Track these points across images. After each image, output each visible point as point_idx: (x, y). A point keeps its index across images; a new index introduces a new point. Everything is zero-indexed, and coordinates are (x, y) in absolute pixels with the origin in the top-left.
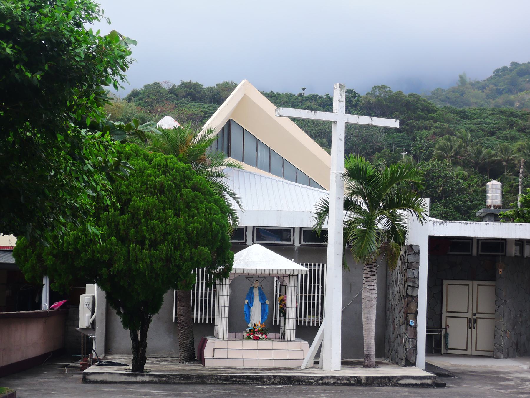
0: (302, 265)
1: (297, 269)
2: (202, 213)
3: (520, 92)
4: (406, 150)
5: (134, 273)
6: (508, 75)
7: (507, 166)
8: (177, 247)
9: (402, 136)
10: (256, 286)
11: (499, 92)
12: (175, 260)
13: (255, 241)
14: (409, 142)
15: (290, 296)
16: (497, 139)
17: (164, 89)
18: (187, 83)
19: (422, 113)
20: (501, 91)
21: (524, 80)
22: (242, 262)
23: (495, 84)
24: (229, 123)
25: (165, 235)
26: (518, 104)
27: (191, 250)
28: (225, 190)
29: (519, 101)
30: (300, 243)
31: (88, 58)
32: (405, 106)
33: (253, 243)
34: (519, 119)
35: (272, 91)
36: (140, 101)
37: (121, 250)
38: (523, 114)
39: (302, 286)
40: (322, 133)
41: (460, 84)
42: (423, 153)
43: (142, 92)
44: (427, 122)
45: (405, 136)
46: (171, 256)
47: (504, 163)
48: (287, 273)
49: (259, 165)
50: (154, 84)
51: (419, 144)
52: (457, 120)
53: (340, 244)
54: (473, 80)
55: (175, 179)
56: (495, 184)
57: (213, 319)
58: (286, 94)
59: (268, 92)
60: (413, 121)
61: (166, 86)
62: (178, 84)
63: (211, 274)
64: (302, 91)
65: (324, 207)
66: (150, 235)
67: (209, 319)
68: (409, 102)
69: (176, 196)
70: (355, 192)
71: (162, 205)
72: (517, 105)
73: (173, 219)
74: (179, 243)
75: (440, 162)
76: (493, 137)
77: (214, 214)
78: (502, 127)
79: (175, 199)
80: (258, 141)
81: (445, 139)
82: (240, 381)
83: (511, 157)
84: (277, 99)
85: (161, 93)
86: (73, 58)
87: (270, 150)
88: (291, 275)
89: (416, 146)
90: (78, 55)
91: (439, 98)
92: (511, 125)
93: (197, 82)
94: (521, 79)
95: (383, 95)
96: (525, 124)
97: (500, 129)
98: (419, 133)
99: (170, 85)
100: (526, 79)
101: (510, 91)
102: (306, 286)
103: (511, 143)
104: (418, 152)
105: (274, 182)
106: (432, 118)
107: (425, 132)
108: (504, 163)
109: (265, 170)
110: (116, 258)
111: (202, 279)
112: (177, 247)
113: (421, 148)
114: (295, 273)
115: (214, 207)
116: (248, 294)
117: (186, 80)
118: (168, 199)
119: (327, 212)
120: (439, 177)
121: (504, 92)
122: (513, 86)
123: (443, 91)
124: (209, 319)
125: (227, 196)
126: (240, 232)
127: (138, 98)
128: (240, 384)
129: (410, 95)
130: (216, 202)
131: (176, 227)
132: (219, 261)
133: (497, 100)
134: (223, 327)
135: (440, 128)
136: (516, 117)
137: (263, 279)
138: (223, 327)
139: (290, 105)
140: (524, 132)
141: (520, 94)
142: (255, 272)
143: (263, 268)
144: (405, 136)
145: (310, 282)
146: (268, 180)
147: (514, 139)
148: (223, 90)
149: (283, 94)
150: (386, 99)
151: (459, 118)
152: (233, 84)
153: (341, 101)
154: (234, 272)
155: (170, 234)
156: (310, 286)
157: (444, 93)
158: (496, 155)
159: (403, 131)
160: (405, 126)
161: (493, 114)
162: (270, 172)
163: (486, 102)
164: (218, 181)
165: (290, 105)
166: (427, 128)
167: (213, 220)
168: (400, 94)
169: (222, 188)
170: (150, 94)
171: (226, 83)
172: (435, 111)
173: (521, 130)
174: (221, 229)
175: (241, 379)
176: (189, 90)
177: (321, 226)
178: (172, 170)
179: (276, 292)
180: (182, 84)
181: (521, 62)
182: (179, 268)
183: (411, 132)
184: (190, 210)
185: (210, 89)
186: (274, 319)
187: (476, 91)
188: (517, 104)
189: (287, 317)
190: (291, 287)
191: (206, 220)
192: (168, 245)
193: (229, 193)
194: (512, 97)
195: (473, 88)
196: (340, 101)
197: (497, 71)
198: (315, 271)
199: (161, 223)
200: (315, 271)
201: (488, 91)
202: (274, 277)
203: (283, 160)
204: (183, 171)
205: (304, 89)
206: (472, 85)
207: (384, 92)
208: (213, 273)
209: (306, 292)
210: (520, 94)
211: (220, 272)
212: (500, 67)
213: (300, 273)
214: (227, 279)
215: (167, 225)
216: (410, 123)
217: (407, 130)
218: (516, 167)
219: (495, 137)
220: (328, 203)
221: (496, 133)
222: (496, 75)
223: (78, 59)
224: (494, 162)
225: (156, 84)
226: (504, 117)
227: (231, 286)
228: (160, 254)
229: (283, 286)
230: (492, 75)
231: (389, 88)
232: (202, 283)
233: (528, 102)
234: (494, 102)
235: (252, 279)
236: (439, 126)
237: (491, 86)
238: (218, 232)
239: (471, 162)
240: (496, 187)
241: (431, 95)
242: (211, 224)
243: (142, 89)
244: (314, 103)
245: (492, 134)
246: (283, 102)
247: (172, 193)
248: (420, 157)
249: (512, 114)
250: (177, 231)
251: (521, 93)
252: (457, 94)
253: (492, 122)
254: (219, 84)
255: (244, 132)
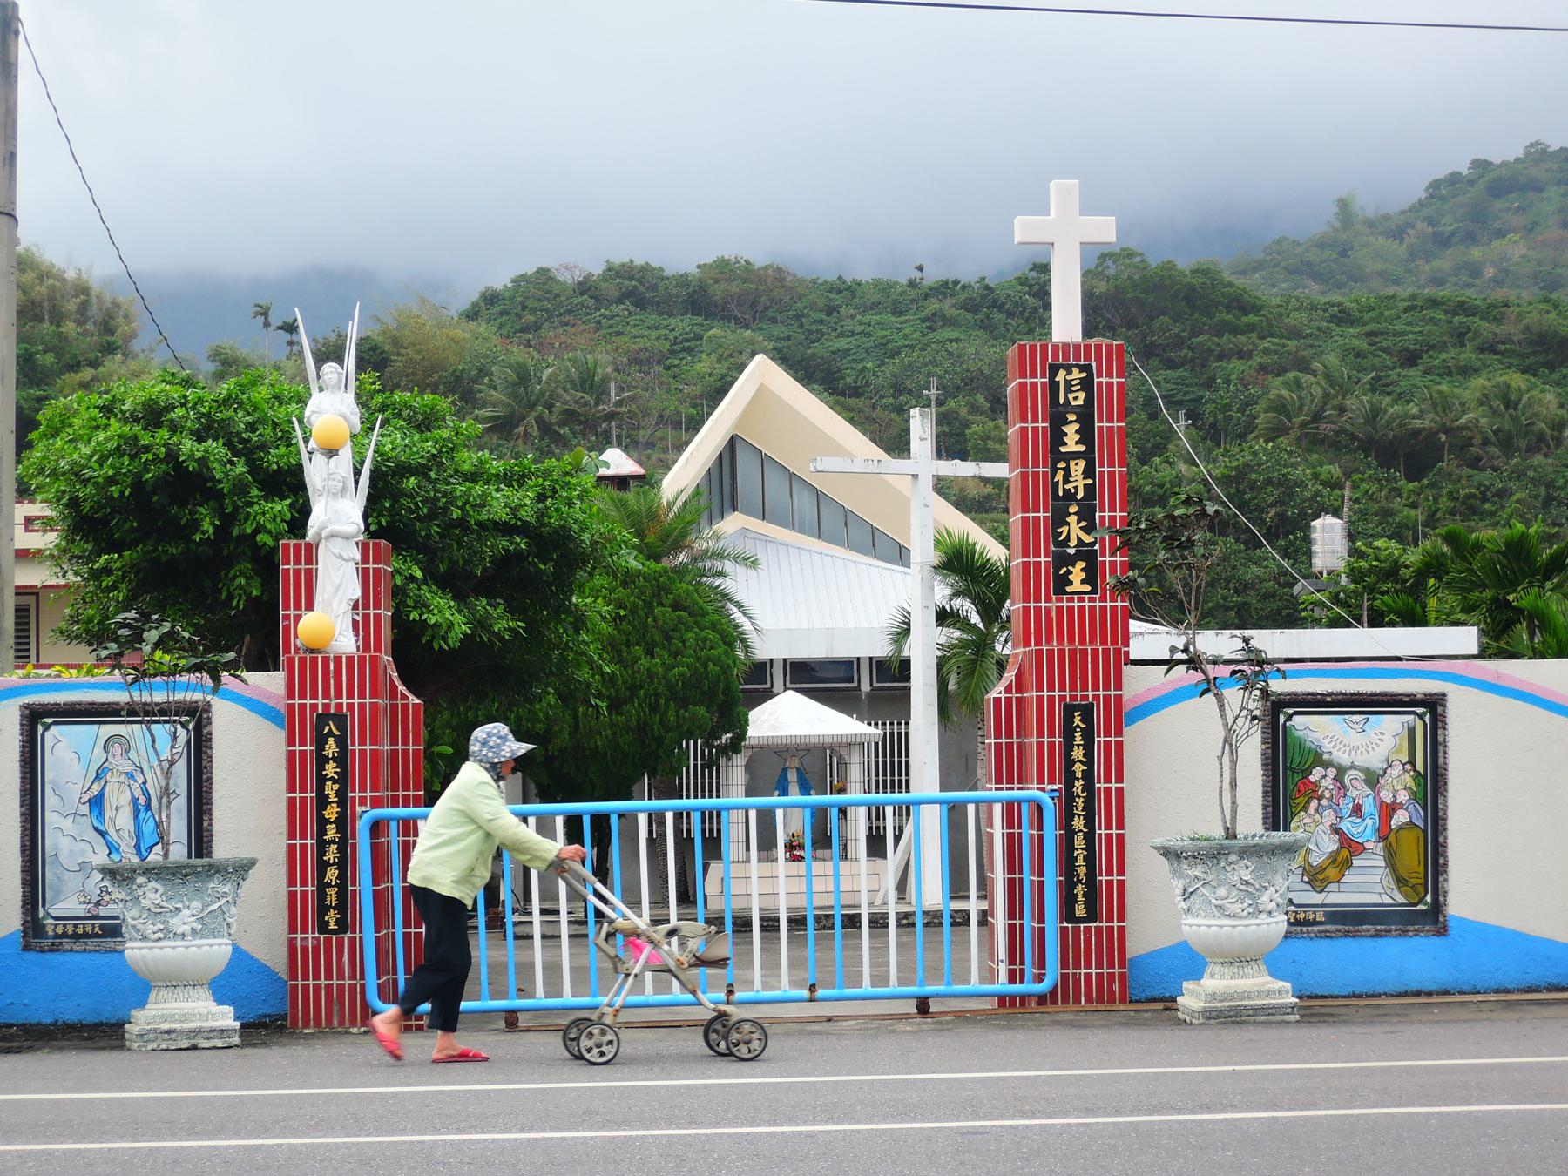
0: (869, 724)
1: (863, 732)
2: (690, 647)
3: (1498, 238)
4: (1188, 416)
5: (587, 753)
6: (1465, 193)
7: (1450, 444)
8: (654, 708)
9: (1179, 377)
10: (792, 766)
11: (1443, 241)
12: (652, 730)
13: (788, 685)
14: (1196, 392)
15: (853, 780)
16: (1425, 373)
17: (565, 283)
18: (623, 265)
19: (1230, 317)
20: (1447, 238)
21: (1507, 205)
22: (765, 725)
23: (1431, 222)
24: (733, 443)
25: (633, 689)
26: (1491, 270)
27: (677, 711)
28: (730, 600)
29: (1493, 264)
30: (871, 685)
31: (594, 543)
32: (1184, 298)
33: (786, 689)
34: (1481, 319)
35: (840, 278)
36: (504, 318)
37: (564, 715)
38: (1490, 306)
39: (877, 763)
40: (972, 380)
41: (1337, 224)
42: (1234, 421)
43: (507, 295)
44: (1242, 338)
45: (1187, 378)
46: (645, 723)
47: (1443, 437)
48: (844, 741)
49: (797, 528)
50: (537, 272)
51: (1222, 398)
52: (1319, 329)
53: (932, 686)
54: (1370, 213)
55: (643, 593)
56: (1331, 524)
57: (719, 831)
58: (877, 283)
59: (830, 280)
60: (1206, 337)
61: (569, 277)
62: (597, 269)
63: (711, 748)
64: (918, 274)
65: (904, 623)
66: (608, 689)
67: (711, 831)
68: (1193, 289)
69: (646, 621)
70: (957, 594)
71: (624, 637)
72: (1489, 273)
73: (644, 662)
74: (657, 702)
75: (1271, 444)
76: (1414, 368)
77: (711, 648)
78: (1439, 342)
79: (645, 625)
80: (792, 476)
81: (1286, 384)
82: (768, 926)
83: (1463, 420)
84: (854, 296)
85: (557, 295)
86: (579, 546)
87: (818, 494)
88: (852, 744)
89: (1214, 402)
90: (583, 541)
91: (1283, 264)
92: (1460, 336)
93: (647, 263)
94: (1499, 204)
95: (1126, 274)
96: (1497, 330)
97: (1432, 347)
98: (1224, 369)
99: (578, 273)
100: (1512, 203)
101: (1471, 238)
102: (884, 763)
103: (1460, 382)
104: (1221, 417)
105: (827, 560)
106: (1251, 328)
107: (1237, 365)
108: (1443, 437)
109: (813, 536)
110: (556, 728)
111: (695, 759)
112: (654, 708)
113: (1228, 407)
114: (858, 741)
115: (711, 635)
116: (779, 781)
117: (620, 258)
118: (634, 627)
119: (908, 631)
120: (1269, 482)
121: (1454, 240)
122: (1478, 222)
123: (1297, 243)
124: (711, 831)
125: (735, 609)
126: (760, 670)
127: (497, 309)
128: (769, 931)
129: (1194, 272)
130: (714, 626)
131: (651, 675)
132: (724, 726)
133: (1437, 263)
134: (736, 840)
135: (1276, 352)
136: (1474, 315)
137: (805, 752)
138: (736, 840)
139: (888, 310)
140: (1495, 352)
141: (1496, 243)
142: (789, 742)
143: (798, 733)
144: (1187, 378)
145: (892, 755)
146: (816, 557)
147: (1467, 371)
148: (716, 281)
149: (867, 282)
150: (1134, 285)
151: (1325, 324)
152: (739, 262)
153: (924, 439)
154: (752, 743)
155: (641, 687)
156: (892, 763)
157: (1298, 250)
158: (1420, 417)
159: (1182, 365)
160: (1185, 351)
161: (1413, 308)
162: (820, 537)
163: (1408, 271)
164: (716, 584)
165: (888, 310)
166: (1242, 355)
167: (709, 659)
168: (1170, 269)
169: (726, 597)
170: (527, 298)
171: (724, 260)
172: (1256, 308)
173: (1486, 349)
174: (724, 673)
175: (770, 923)
176: (627, 282)
177: (899, 653)
178: (638, 578)
179: (831, 776)
180: (609, 270)
181: (1497, 160)
182: (659, 741)
183: (1204, 366)
184: (669, 643)
185: (683, 280)
186: (829, 826)
187: (1382, 241)
188: (1490, 272)
189: (849, 818)
190: (853, 766)
191: (698, 659)
192: (640, 704)
193: (738, 605)
194: (1476, 253)
195: (1372, 233)
196: (922, 440)
197: (1436, 184)
198: (900, 734)
199: (625, 669)
200: (900, 734)
201: (1414, 240)
202: (824, 749)
203: (846, 512)
204: (655, 579)
205: (920, 268)
206: (1371, 224)
207: (1127, 266)
208: (714, 747)
209: (885, 774)
210: (1497, 244)
211: (726, 744)
212: (1441, 173)
213: (872, 739)
214: (739, 756)
215: (634, 673)
216: (1199, 343)
217: (1192, 360)
218: (1473, 446)
219: (1421, 368)
220: (909, 613)
221: (1421, 358)
222: (1432, 197)
223: (584, 546)
224: (1416, 433)
225: (543, 272)
226: (1443, 317)
227: (748, 767)
228: (628, 721)
229: (842, 764)
230: (1423, 195)
231: (1141, 255)
232: (695, 766)
233: (1517, 263)
234: (1427, 268)
235: (784, 755)
236: (1272, 347)
237: (1420, 226)
238: (719, 679)
239: (1353, 437)
240: (1332, 531)
241: (1261, 256)
242: (706, 667)
243: (506, 286)
244: (948, 302)
245: (1411, 359)
246: (869, 303)
247: (639, 617)
248: (1226, 430)
249: (1462, 308)
250: (652, 682)
251: (1498, 241)
252: (1328, 254)
253: (1411, 333)
254: (704, 265)
255: (764, 460)
